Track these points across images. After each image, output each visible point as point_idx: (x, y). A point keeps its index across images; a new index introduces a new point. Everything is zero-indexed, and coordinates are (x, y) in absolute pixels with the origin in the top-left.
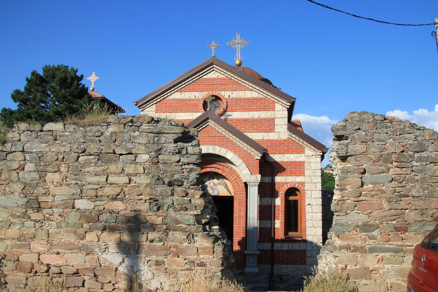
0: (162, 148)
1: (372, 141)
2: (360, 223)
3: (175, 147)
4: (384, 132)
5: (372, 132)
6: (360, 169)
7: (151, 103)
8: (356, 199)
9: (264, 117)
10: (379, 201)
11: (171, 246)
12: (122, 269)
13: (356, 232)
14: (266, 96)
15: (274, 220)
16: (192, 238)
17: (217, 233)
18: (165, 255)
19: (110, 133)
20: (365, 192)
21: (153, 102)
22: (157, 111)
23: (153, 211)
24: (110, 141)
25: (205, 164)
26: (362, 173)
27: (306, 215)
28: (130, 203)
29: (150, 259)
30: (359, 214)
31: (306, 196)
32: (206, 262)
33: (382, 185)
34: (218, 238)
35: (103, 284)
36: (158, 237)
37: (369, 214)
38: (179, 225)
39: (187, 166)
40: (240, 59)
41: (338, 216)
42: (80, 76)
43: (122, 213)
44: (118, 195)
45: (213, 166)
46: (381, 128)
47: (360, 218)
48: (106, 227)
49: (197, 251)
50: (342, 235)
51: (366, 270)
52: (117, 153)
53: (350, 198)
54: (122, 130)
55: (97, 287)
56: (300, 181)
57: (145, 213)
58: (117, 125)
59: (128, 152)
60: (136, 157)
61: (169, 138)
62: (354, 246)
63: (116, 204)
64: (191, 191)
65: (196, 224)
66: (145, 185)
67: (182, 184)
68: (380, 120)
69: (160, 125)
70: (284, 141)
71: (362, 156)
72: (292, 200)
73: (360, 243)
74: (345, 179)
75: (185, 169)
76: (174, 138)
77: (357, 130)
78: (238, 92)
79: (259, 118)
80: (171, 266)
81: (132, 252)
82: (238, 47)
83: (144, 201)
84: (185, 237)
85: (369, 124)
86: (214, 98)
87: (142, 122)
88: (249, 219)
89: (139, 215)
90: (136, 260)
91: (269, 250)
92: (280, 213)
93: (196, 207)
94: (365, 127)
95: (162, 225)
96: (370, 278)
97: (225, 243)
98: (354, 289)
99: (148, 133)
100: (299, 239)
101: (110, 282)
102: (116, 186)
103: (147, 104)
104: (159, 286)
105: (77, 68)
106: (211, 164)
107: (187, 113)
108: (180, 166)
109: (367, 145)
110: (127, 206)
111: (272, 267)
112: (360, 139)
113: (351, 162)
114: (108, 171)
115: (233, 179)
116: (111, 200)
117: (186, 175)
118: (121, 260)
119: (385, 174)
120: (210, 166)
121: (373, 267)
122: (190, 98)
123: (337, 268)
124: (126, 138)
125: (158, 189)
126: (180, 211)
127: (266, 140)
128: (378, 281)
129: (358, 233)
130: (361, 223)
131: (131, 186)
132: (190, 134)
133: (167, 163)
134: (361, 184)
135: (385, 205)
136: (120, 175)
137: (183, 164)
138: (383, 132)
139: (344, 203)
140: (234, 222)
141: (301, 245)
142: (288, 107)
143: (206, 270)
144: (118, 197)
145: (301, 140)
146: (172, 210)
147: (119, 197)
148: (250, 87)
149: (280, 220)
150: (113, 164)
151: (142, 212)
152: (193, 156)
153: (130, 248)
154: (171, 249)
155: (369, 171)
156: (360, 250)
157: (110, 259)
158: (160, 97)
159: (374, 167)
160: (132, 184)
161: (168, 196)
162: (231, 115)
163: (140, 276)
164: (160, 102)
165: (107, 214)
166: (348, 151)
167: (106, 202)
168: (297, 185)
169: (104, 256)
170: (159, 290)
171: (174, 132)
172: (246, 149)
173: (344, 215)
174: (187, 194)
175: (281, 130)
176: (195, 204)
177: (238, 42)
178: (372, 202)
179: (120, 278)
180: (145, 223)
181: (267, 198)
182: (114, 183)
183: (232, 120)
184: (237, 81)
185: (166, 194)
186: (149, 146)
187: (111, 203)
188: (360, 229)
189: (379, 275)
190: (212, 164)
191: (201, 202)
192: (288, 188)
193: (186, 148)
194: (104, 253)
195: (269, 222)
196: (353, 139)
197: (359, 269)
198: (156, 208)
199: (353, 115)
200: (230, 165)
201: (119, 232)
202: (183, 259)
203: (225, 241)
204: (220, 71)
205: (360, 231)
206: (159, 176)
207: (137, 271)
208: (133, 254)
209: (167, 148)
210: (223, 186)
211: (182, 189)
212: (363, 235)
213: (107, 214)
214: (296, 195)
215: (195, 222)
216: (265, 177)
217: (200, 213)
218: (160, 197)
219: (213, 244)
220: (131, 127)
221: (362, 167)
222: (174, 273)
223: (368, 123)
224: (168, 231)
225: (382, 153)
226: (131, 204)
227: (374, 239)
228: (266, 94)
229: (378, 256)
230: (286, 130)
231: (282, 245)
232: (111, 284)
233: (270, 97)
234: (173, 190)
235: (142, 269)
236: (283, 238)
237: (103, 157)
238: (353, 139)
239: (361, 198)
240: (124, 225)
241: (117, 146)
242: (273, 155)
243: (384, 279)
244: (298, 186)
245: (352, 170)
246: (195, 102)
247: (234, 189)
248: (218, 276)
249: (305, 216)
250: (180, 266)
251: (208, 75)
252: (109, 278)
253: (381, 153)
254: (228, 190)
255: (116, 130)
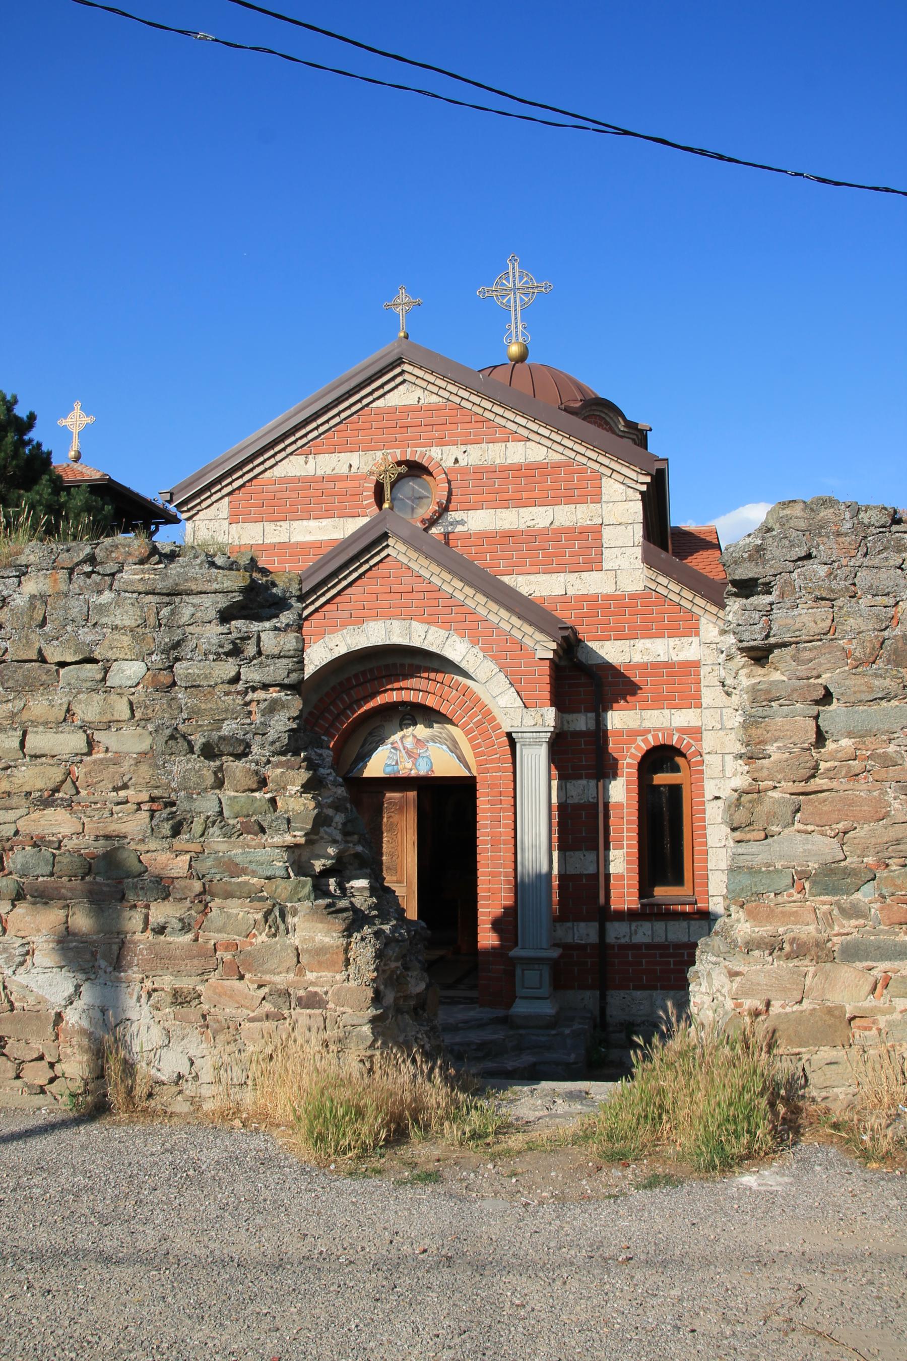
0: (183, 640)
1: (852, 594)
2: (813, 866)
3: (222, 634)
4: (892, 563)
5: (852, 564)
6: (811, 689)
7: (215, 493)
8: (801, 787)
9: (568, 524)
10: (875, 793)
11: (218, 946)
12: (73, 1017)
13: (799, 893)
14: (572, 455)
15: (607, 848)
16: (279, 919)
17: (366, 901)
18: (200, 972)
19: (27, 598)
20: (829, 765)
21: (220, 490)
22: (234, 519)
23: (160, 836)
24: (29, 623)
25: (384, 680)
26: (818, 702)
27: (708, 832)
28: (92, 814)
29: (156, 986)
30: (809, 836)
31: (708, 773)
32: (326, 993)
33: (885, 738)
34: (367, 916)
35: (21, 1063)
36: (176, 918)
37: (841, 834)
38: (240, 879)
39: (260, 695)
40: (521, 340)
41: (739, 842)
42: (25, 418)
43: (69, 845)
44: (56, 790)
45: (408, 683)
46: (879, 552)
47: (814, 848)
48: (23, 890)
49: (296, 959)
50: (754, 904)
51: (832, 1015)
52: (49, 659)
53: (778, 785)
54: (63, 587)
55: (4, 1071)
56: (686, 724)
57: (137, 844)
58: (48, 572)
59: (81, 657)
60: (106, 671)
61: (202, 608)
62: (794, 939)
63: (50, 818)
64: (273, 773)
65: (292, 874)
66: (135, 756)
67: (245, 749)
68: (877, 524)
69: (174, 569)
70: (633, 597)
71: (819, 646)
72: (665, 786)
73: (812, 928)
74: (761, 722)
75: (255, 704)
76: (220, 606)
77: (800, 559)
78: (484, 446)
79: (552, 526)
80: (218, 1005)
81: (103, 963)
82: (515, 302)
83: (135, 807)
84: (259, 916)
85: (840, 540)
86: (403, 469)
87: (121, 559)
88: (522, 849)
89: (121, 850)
90: (113, 989)
91: (592, 946)
92: (625, 826)
93: (289, 821)
94: (825, 548)
95: (188, 881)
96: (845, 1043)
97: (388, 932)
98: (793, 1078)
99: (140, 593)
100: (688, 908)
101: (41, 1058)
102: (51, 762)
103: (202, 498)
104: (184, 1069)
105: (14, 393)
106: (403, 680)
107: (325, 522)
108: (238, 693)
109: (836, 609)
110: (84, 824)
111: (603, 997)
112: (809, 590)
113: (781, 666)
114: (25, 716)
115: (472, 725)
116: (35, 805)
117: (258, 722)
118: (72, 989)
119: (897, 703)
120: (401, 684)
121: (855, 1007)
122: (334, 472)
123: (738, 1010)
124: (74, 612)
125: (175, 769)
126: (242, 834)
127: (576, 596)
128: (872, 1052)
129: (807, 896)
130: (816, 866)
131: (95, 762)
132: (274, 590)
133: (199, 686)
134: (817, 738)
135: (896, 806)
136: (60, 729)
137: (247, 688)
138: (886, 564)
139: (759, 801)
140: (479, 858)
141: (692, 928)
142: (644, 488)
143: (325, 1020)
144: (56, 794)
145: (687, 594)
146: (218, 832)
147: (61, 795)
148: (522, 431)
149: (625, 850)
150: (38, 695)
151: (128, 840)
152: (277, 661)
153: (96, 951)
154: (218, 953)
155: (842, 694)
156: (813, 953)
157: (39, 987)
158: (240, 473)
159: (860, 680)
160: (98, 755)
161: (205, 790)
162: (462, 522)
163: (128, 1038)
164: (243, 489)
165: (27, 848)
166: (771, 629)
167: (23, 811)
168: (675, 738)
169: (21, 978)
170: (187, 1081)
171: (217, 587)
172: (507, 627)
173: (758, 838)
174: (263, 783)
175: (624, 563)
176: (287, 812)
177: (514, 285)
178: (852, 797)
179: (68, 1045)
180: (140, 875)
181: (584, 782)
182: (42, 752)
183: (468, 536)
184: (480, 411)
185: (198, 784)
186: (143, 634)
187: (36, 815)
188: (814, 884)
189: (874, 1031)
190: (406, 677)
191: (305, 805)
192: (649, 747)
193: (256, 636)
194: (21, 970)
195: (591, 856)
196: (789, 589)
197: (811, 1014)
198: (169, 827)
199: (787, 512)
200: (460, 679)
201: (61, 903)
202: (256, 986)
203: (387, 928)
204: (424, 384)
205: (813, 891)
206: (176, 729)
207: (116, 1026)
208: (105, 972)
209: (199, 639)
210: (444, 747)
211: (248, 765)
212: (824, 903)
213: (27, 848)
214: (676, 769)
215: (290, 870)
216: (575, 716)
217: (302, 840)
218: (182, 793)
219: (343, 936)
220: (89, 577)
221: (820, 681)
222: (229, 1028)
223: (838, 534)
224: (209, 898)
225: (886, 634)
226: (96, 817)
227: (858, 917)
228: (572, 449)
229: (873, 972)
230: (639, 564)
231: (633, 928)
232: (44, 1064)
233: (584, 460)
234: (220, 768)
235: (134, 1018)
236: (636, 905)
237: (10, 674)
238: (789, 589)
239: (818, 783)
240: (76, 883)
241: (50, 640)
242: (597, 643)
243: (893, 1046)
244: (681, 740)
245: (783, 694)
246: (350, 484)
247: (476, 755)
248: (362, 1038)
249: (705, 836)
250: (247, 1008)
251: (388, 396)
252: (38, 1046)
253: (882, 633)
254: (462, 759)
255: (45, 588)
